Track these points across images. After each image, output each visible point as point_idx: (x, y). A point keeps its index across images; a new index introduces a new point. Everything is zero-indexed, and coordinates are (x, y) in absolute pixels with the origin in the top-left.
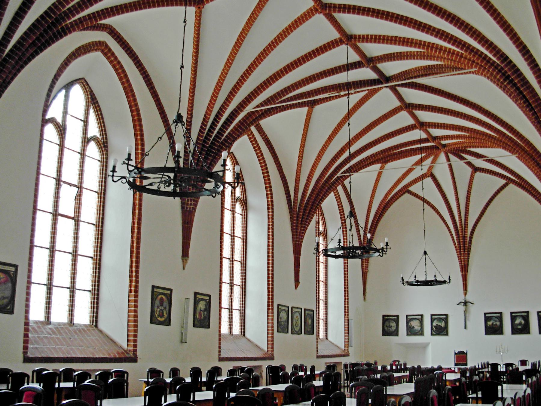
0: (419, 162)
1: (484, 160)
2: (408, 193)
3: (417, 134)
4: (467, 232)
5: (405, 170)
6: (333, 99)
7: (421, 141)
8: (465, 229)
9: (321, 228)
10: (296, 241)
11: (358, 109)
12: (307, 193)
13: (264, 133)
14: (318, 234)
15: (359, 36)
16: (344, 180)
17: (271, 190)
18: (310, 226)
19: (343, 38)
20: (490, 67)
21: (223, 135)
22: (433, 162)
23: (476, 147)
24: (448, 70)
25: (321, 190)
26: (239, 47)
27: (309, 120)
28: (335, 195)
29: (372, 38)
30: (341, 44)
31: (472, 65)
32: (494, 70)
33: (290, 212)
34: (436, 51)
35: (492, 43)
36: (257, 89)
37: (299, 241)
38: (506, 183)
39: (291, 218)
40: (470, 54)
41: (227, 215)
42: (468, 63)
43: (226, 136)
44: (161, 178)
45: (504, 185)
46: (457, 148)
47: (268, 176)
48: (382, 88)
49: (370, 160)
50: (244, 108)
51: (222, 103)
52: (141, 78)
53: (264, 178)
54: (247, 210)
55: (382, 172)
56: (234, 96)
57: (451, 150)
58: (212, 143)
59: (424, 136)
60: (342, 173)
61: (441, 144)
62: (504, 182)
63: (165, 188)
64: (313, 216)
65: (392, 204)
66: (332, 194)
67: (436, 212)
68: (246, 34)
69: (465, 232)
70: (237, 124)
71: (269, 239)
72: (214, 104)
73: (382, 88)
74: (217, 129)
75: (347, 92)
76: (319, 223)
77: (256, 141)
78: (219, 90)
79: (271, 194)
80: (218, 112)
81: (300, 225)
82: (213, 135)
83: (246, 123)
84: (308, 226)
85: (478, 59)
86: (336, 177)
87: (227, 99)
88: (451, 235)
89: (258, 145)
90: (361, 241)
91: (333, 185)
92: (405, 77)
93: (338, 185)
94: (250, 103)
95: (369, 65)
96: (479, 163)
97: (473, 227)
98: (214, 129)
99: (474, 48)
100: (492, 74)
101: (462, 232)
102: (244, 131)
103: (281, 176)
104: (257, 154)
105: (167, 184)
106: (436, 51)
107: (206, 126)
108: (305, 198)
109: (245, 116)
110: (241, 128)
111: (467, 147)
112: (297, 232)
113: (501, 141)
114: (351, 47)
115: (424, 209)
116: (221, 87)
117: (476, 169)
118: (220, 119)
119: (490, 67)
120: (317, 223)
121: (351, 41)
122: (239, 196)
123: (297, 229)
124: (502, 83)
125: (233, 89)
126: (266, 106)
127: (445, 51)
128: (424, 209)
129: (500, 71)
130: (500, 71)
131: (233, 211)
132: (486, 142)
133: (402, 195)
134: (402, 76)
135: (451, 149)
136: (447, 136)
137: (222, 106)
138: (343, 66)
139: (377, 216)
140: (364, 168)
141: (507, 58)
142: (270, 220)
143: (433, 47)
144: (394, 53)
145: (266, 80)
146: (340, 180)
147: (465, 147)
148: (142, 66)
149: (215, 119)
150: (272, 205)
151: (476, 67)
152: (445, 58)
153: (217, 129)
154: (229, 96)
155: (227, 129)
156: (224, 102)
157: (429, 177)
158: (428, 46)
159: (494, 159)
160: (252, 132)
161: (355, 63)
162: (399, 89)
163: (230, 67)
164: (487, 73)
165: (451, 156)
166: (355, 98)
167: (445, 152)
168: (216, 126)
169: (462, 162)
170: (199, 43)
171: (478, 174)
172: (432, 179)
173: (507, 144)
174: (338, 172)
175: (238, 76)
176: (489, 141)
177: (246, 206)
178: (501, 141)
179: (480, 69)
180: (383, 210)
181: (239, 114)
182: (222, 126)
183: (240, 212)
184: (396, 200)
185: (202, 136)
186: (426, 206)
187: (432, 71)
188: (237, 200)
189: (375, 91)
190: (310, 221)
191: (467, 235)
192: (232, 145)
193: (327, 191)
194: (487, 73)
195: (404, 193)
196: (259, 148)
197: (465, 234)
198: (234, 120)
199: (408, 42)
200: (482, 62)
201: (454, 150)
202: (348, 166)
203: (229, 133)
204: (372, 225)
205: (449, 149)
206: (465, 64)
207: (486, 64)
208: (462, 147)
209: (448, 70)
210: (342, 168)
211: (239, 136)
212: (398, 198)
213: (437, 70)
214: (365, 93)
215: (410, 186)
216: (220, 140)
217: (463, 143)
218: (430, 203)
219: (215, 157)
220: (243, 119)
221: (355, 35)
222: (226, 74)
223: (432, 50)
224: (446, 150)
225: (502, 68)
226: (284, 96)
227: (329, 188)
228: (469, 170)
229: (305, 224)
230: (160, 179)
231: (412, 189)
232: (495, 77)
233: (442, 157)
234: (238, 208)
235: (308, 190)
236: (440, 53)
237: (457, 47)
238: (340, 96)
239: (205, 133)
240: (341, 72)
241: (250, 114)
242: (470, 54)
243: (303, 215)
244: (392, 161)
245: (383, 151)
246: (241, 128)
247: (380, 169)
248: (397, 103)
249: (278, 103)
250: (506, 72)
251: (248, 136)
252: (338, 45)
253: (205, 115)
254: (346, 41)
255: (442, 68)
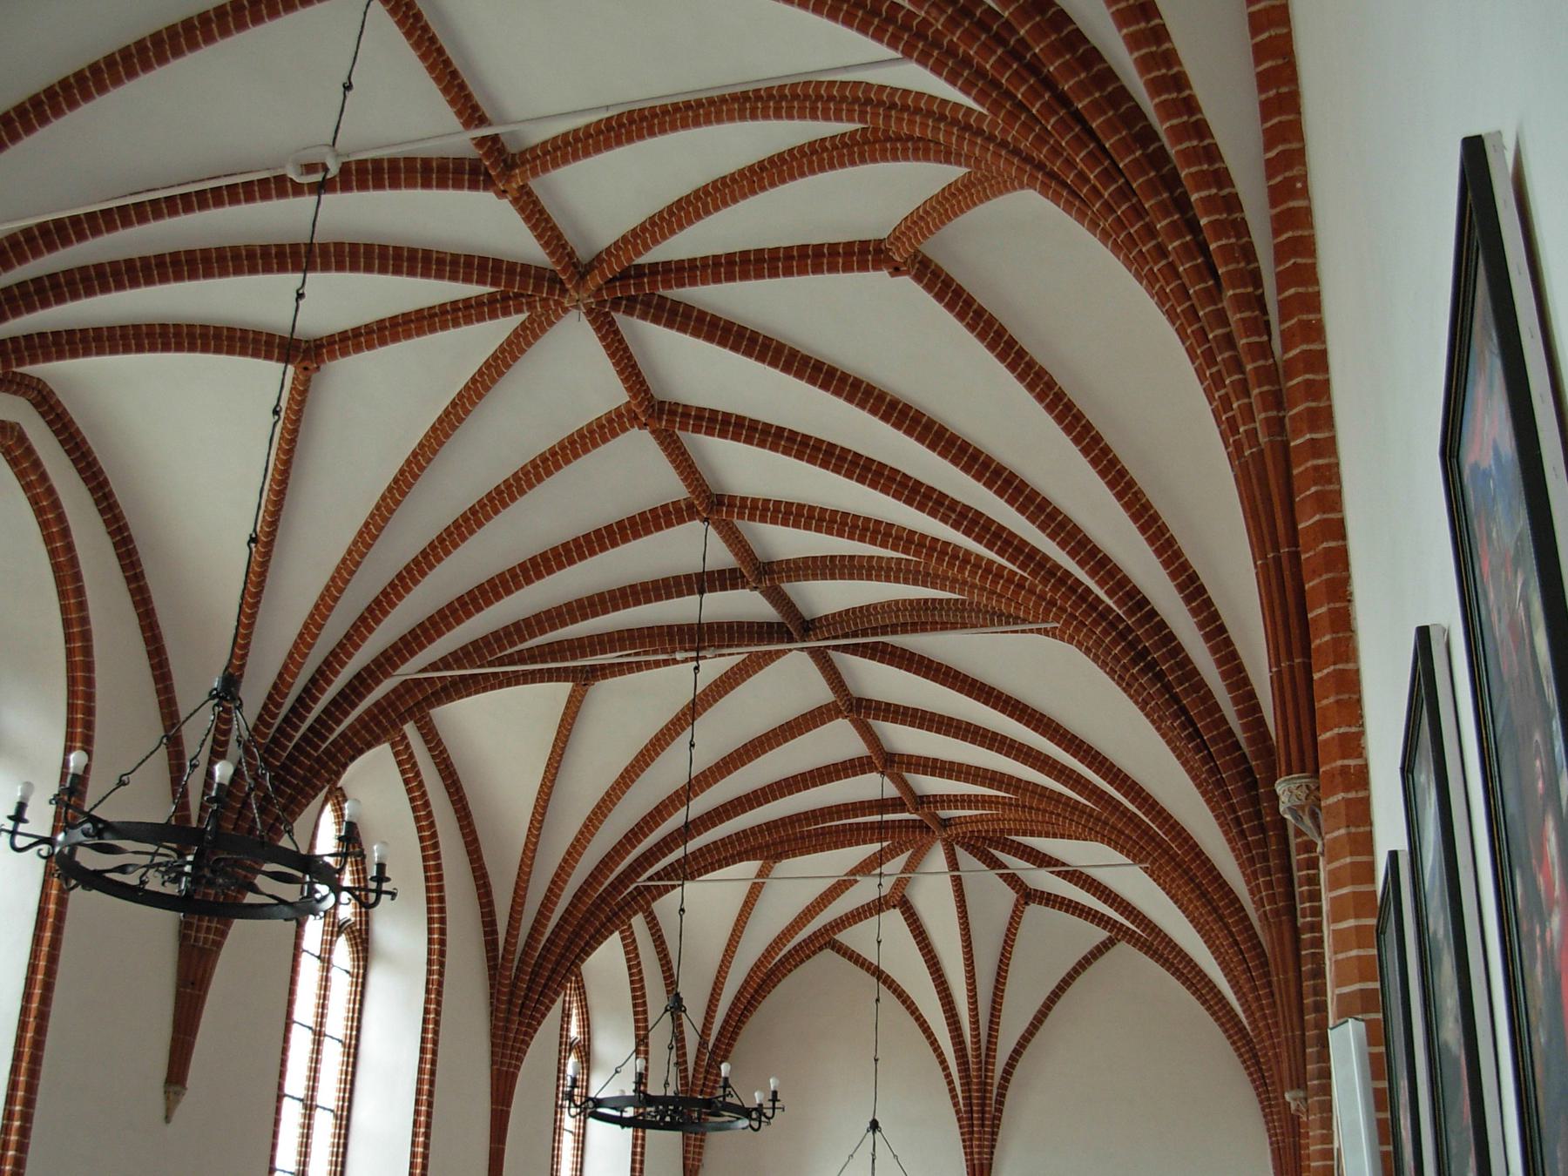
0: (865, 868)
1: (1052, 872)
2: (833, 949)
3: (871, 786)
4: (993, 1071)
5: (823, 886)
6: (631, 671)
7: (882, 805)
8: (986, 1063)
9: (574, 1031)
10: (502, 1064)
11: (716, 701)
12: (545, 926)
13: (440, 742)
14: (566, 1047)
15: (744, 499)
16: (654, 899)
17: (442, 910)
18: (545, 1022)
19: (696, 502)
20: (1096, 623)
21: (324, 739)
22: (911, 867)
23: (1032, 835)
24: (985, 619)
25: (587, 921)
26: (404, 494)
27: (574, 719)
28: (623, 939)
29: (777, 510)
30: (691, 519)
31: (1047, 611)
32: (1106, 632)
33: (492, 977)
34: (951, 565)
35: (1106, 560)
36: (427, 624)
37: (509, 1065)
38: (1110, 938)
39: (492, 995)
40: (1045, 581)
41: (309, 969)
42: (1037, 605)
43: (334, 743)
44: (154, 854)
45: (1103, 943)
46: (979, 831)
47: (438, 867)
48: (790, 650)
49: (733, 847)
50: (395, 667)
51: (333, 644)
52: (106, 544)
53: (425, 872)
54: (366, 960)
55: (764, 883)
56: (371, 630)
57: (964, 837)
58: (290, 756)
59: (891, 791)
60: (650, 879)
61: (935, 816)
62: (1102, 934)
63: (163, 884)
64: (558, 994)
65: (784, 975)
66: (616, 937)
67: (908, 1008)
68: (429, 461)
69: (987, 1070)
70: (368, 711)
71: (423, 1050)
72: (310, 646)
73: (790, 650)
74: (311, 718)
75: (694, 654)
76: (569, 1016)
77: (415, 765)
78: (330, 609)
79: (442, 921)
80: (319, 671)
81: (516, 1018)
82: (298, 736)
83: (395, 710)
84: (539, 1023)
85: (1065, 597)
86: (632, 887)
87: (348, 636)
88: (948, 1076)
89: (418, 774)
90: (686, 1077)
91: (621, 909)
92: (842, 629)
93: (635, 913)
94: (413, 653)
95: (760, 582)
96: (1044, 880)
97: (1011, 1057)
98: (303, 719)
99: (1058, 567)
100: (1099, 643)
101: (980, 1069)
102: (385, 731)
103: (474, 870)
104: (412, 800)
105: (173, 875)
106: (951, 565)
107: (279, 706)
108: (538, 941)
109: (394, 690)
110: (379, 724)
111: (1010, 832)
112: (506, 1038)
113: (1106, 823)
114: (716, 528)
115: (878, 1000)
116: (336, 599)
117: (1028, 895)
118: (322, 691)
119: (1096, 623)
120: (566, 1016)
121: (719, 512)
122: (349, 917)
123: (507, 1029)
124: (1126, 668)
125: (369, 609)
126: (459, 668)
127: (977, 566)
128: (878, 1000)
129: (1122, 636)
130: (1122, 636)
131: (326, 961)
132: (1064, 822)
133: (814, 953)
134: (848, 623)
135: (964, 833)
136: (955, 796)
137: (333, 653)
138: (688, 577)
139: (739, 1008)
140: (714, 870)
141: (1145, 601)
142: (433, 996)
143: (943, 552)
144: (833, 558)
145: (574, 540)
146: (644, 897)
147: (1002, 831)
148: (117, 511)
149: (306, 690)
150: (442, 953)
151: (1057, 618)
152: (973, 586)
153: (311, 718)
154: (355, 627)
155: (339, 722)
156: (341, 645)
157: (894, 907)
158: (932, 549)
159: (984, 867)
160: (404, 737)
161: (721, 572)
162: (832, 653)
163: (369, 546)
164: (1088, 637)
165: (961, 853)
166: (715, 666)
167: (944, 840)
168: (309, 710)
169: (992, 876)
170: (289, 468)
171: (1033, 910)
172: (903, 913)
173: (1121, 832)
174: (639, 875)
175: (389, 575)
176: (1072, 820)
177: (366, 950)
178: (1106, 823)
179: (1067, 624)
180: (756, 991)
181: (378, 682)
182: (326, 711)
183: (348, 965)
184: (796, 966)
185: (264, 736)
186: (886, 994)
187: (933, 615)
188: (340, 927)
189: (771, 657)
190: (548, 1009)
191: (992, 1078)
192: (345, 766)
193: (603, 925)
194: (1088, 637)
195: (821, 949)
196: (421, 785)
197: (986, 1077)
198: (361, 697)
199: (876, 532)
200: (1076, 606)
201: (970, 838)
202: (678, 854)
203: (342, 735)
204: (720, 1033)
205: (957, 835)
206: (1027, 607)
207: (1086, 614)
208: (994, 831)
209: (985, 619)
210: (651, 865)
211: (370, 746)
212: (802, 961)
213: (947, 615)
214: (738, 658)
215: (840, 931)
216: (316, 751)
217: (993, 819)
218: (893, 981)
219: (295, 798)
220: (386, 697)
221: (732, 498)
222: (358, 564)
223: (940, 560)
224: (950, 836)
225: (1129, 629)
226: (513, 644)
227: (609, 919)
228: (1011, 896)
229: (532, 1017)
230: (149, 857)
231: (845, 937)
232: (1108, 651)
233: (937, 858)
234: (343, 952)
235: (548, 919)
236: (961, 569)
237: (1012, 560)
238: (675, 662)
239: (281, 717)
240: (680, 594)
241: (408, 687)
242: (1045, 581)
243: (529, 989)
244: (794, 856)
245: (771, 826)
246: (379, 724)
247: (758, 876)
248: (822, 693)
249: (491, 664)
250: (1138, 640)
251: (393, 746)
252: (681, 521)
253: (280, 675)
254: (704, 510)
255: (964, 610)
